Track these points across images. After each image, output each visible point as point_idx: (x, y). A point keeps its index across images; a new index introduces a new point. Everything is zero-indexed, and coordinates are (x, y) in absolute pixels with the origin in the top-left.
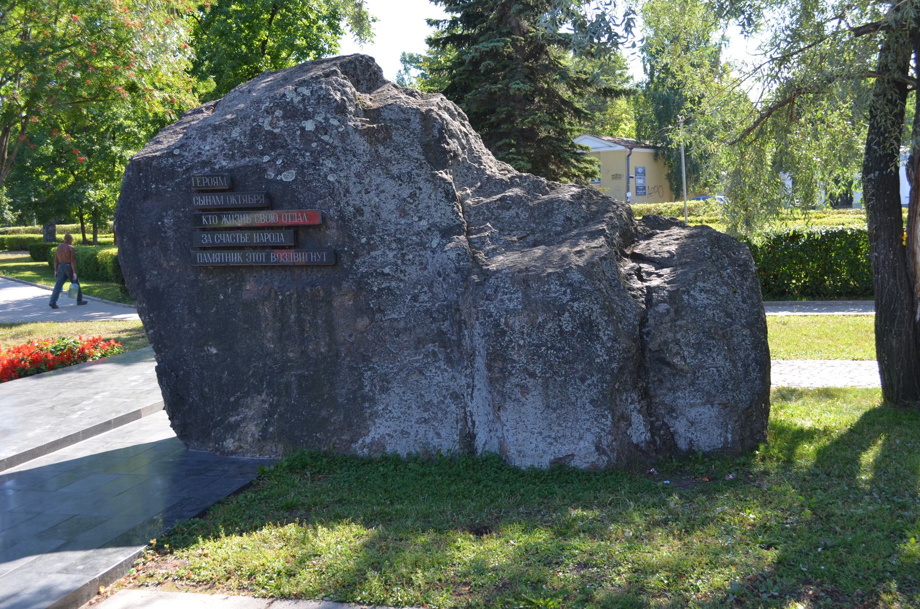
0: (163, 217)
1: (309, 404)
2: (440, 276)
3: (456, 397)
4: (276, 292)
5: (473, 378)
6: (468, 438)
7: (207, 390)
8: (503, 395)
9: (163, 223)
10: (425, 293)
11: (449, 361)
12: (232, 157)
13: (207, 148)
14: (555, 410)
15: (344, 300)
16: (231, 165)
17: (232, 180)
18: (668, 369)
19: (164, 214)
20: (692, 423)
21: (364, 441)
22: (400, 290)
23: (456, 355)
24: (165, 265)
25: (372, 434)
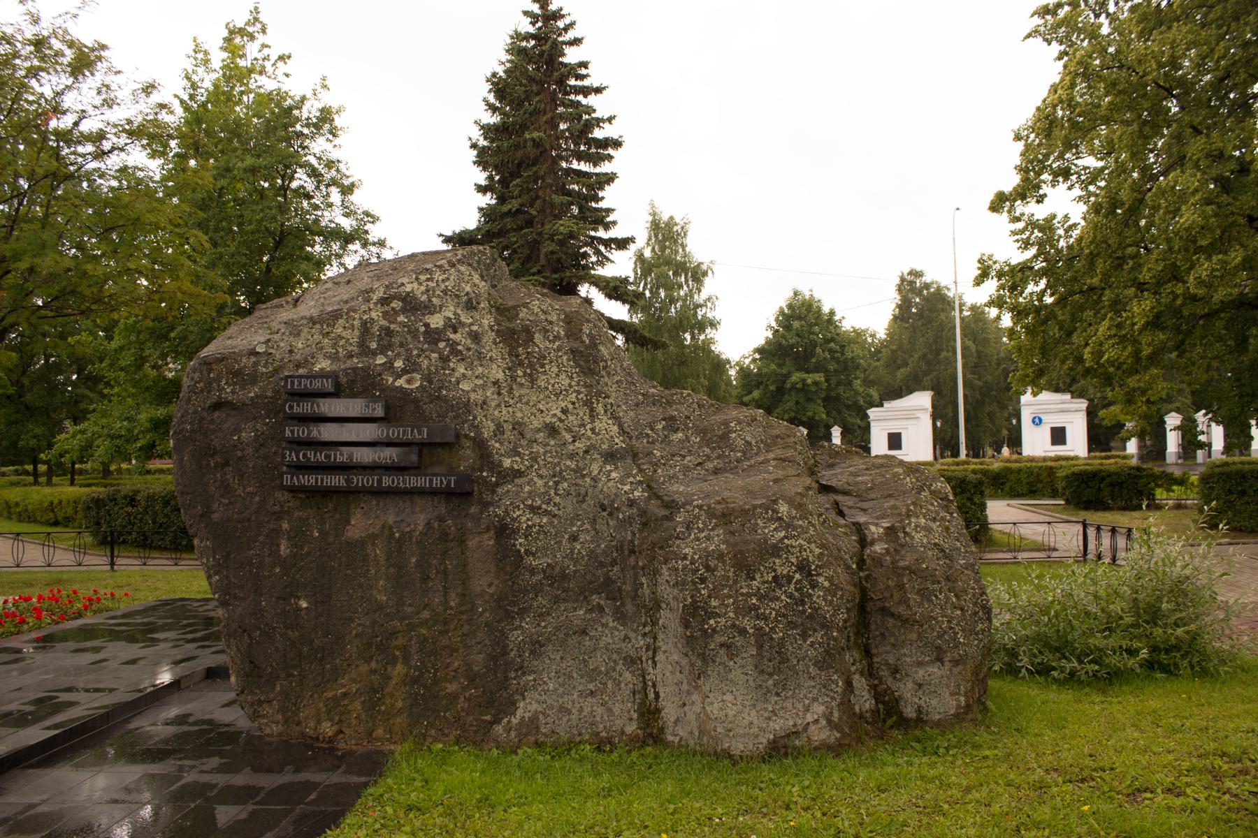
2: (604, 510)
3: (631, 661)
5: (655, 639)
8: (703, 657)
10: (587, 531)
11: (621, 617)
13: (300, 345)
14: (771, 675)
16: (334, 367)
17: (337, 385)
18: (891, 620)
20: (920, 686)
21: (509, 722)
22: (554, 527)
23: (629, 608)
25: (519, 713)
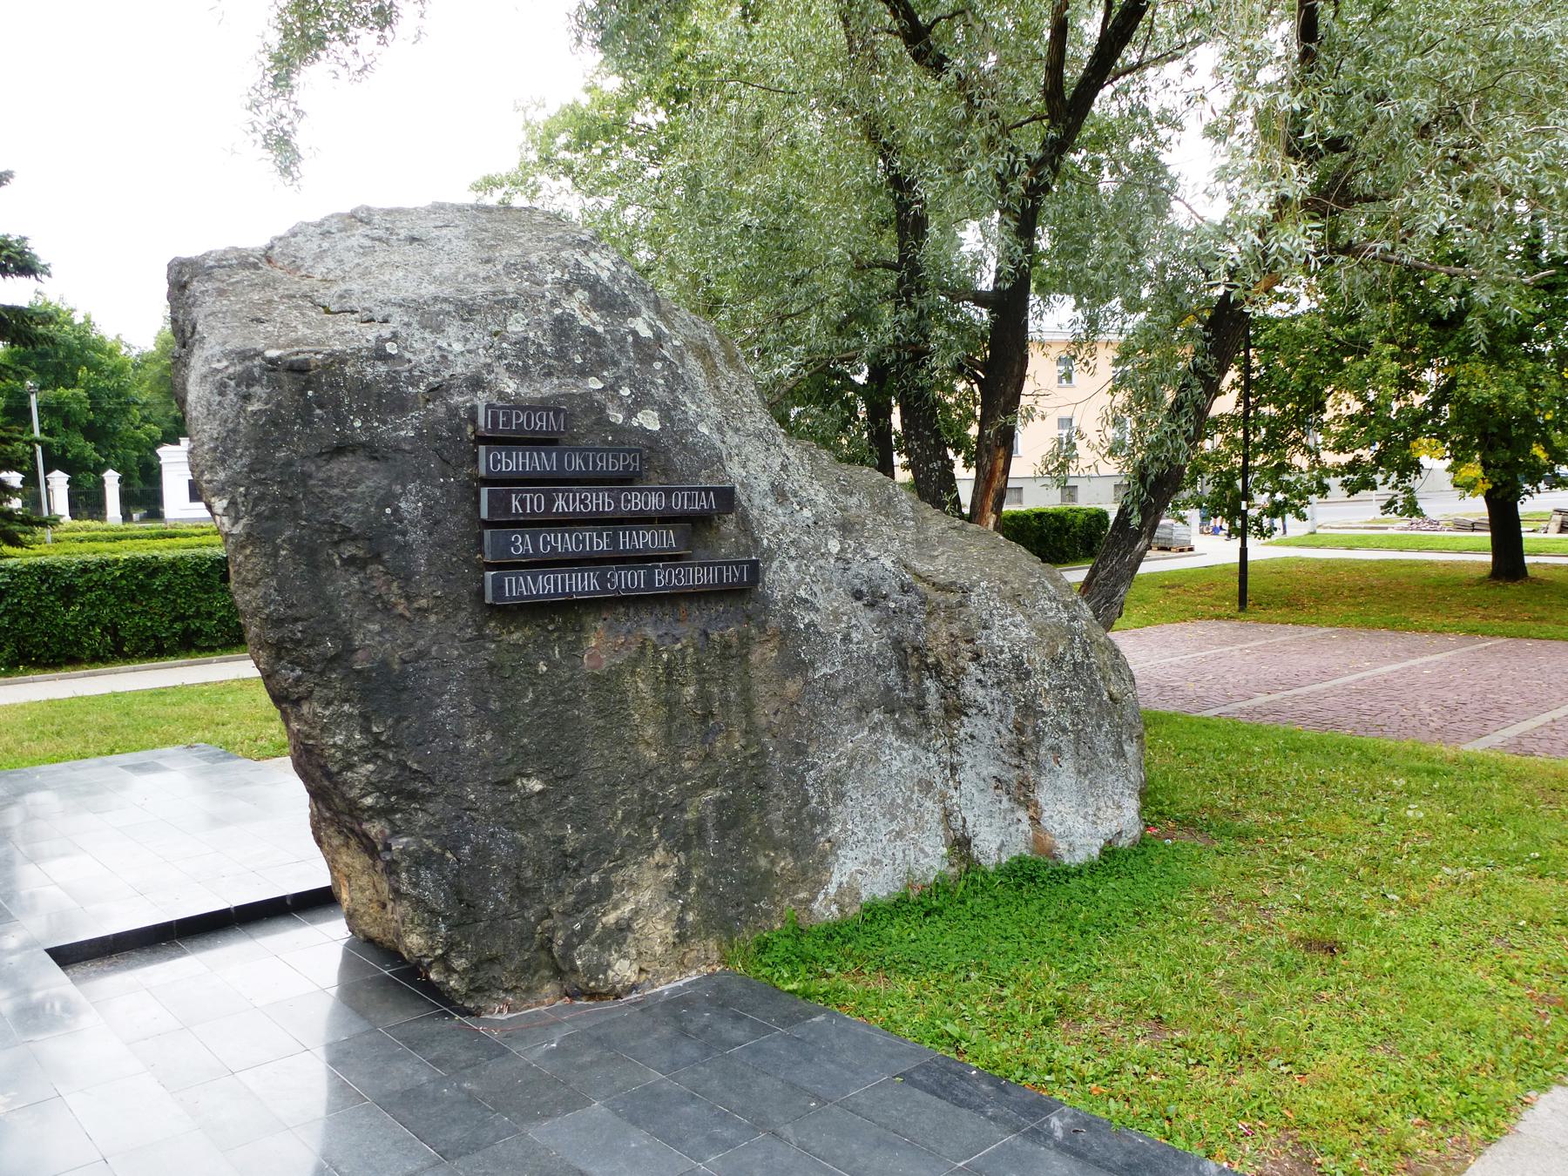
0: (397, 497)
1: (739, 850)
4: (655, 646)
6: (961, 845)
7: (529, 873)
9: (396, 511)
12: (523, 373)
15: (764, 654)
19: (398, 489)
21: (826, 894)
24: (400, 609)
25: (836, 879)
